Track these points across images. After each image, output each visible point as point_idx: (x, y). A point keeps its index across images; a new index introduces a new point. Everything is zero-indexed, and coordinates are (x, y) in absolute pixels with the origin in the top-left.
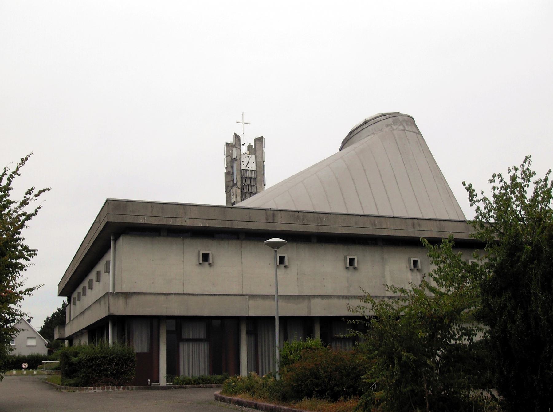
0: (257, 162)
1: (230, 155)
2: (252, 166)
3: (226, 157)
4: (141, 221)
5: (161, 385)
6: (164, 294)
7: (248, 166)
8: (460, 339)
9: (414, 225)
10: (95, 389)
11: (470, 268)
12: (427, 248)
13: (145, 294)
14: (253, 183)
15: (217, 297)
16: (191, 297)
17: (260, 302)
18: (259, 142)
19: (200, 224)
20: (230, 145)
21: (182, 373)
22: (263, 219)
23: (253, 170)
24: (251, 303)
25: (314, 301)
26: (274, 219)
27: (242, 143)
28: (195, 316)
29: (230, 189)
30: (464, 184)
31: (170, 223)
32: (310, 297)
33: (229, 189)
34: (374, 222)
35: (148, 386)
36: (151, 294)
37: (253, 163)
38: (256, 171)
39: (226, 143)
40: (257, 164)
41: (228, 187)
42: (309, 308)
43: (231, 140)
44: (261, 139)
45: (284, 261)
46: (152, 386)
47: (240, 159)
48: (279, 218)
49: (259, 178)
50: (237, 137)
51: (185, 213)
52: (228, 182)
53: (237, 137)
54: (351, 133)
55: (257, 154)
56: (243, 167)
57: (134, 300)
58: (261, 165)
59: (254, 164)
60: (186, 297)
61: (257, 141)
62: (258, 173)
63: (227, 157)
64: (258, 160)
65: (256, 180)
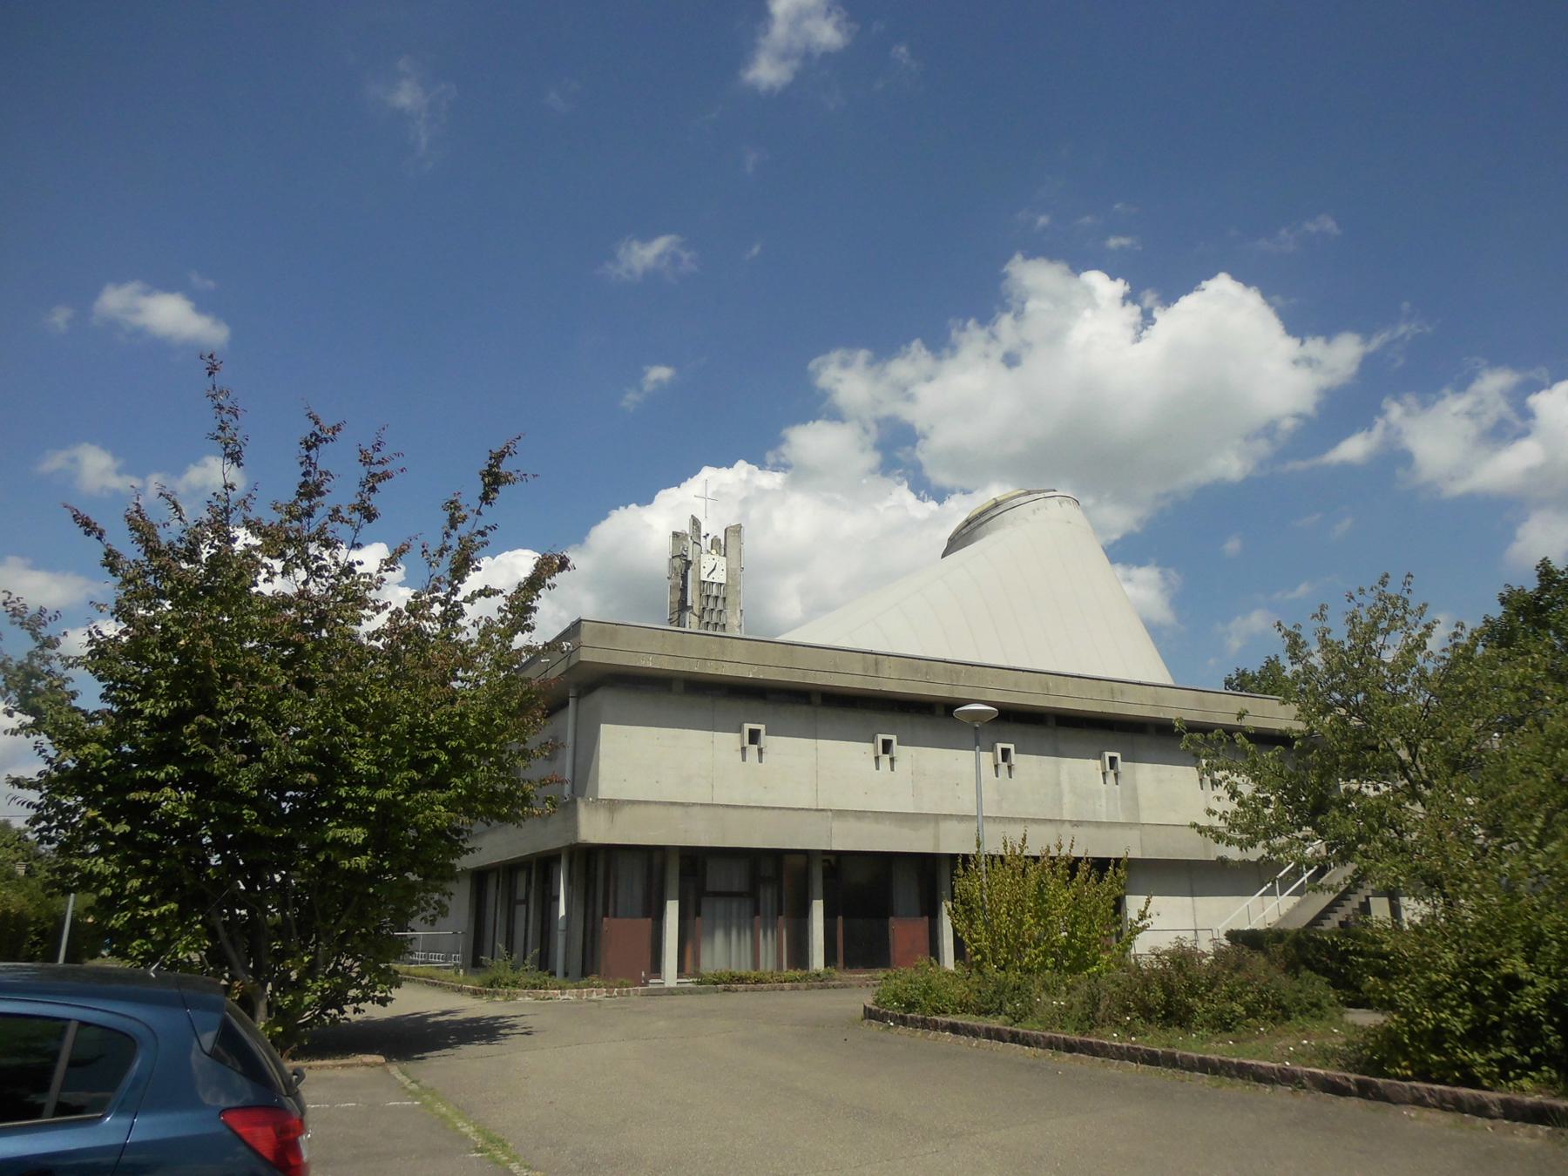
2: (720, 577)
4: (642, 663)
5: (666, 985)
6: (682, 804)
7: (711, 576)
9: (1112, 691)
10: (564, 994)
11: (546, 791)
13: (646, 803)
14: (720, 606)
15: (776, 812)
16: (731, 811)
17: (851, 824)
19: (749, 673)
22: (858, 669)
23: (721, 584)
24: (838, 826)
25: (946, 826)
26: (877, 671)
27: (703, 534)
31: (696, 669)
32: (937, 818)
34: (1047, 684)
36: (656, 803)
38: (727, 585)
42: (937, 838)
43: (686, 528)
45: (595, 755)
46: (650, 986)
47: (699, 561)
48: (888, 670)
50: (695, 522)
51: (723, 653)
53: (695, 522)
54: (969, 523)
56: (704, 578)
57: (626, 815)
60: (721, 811)
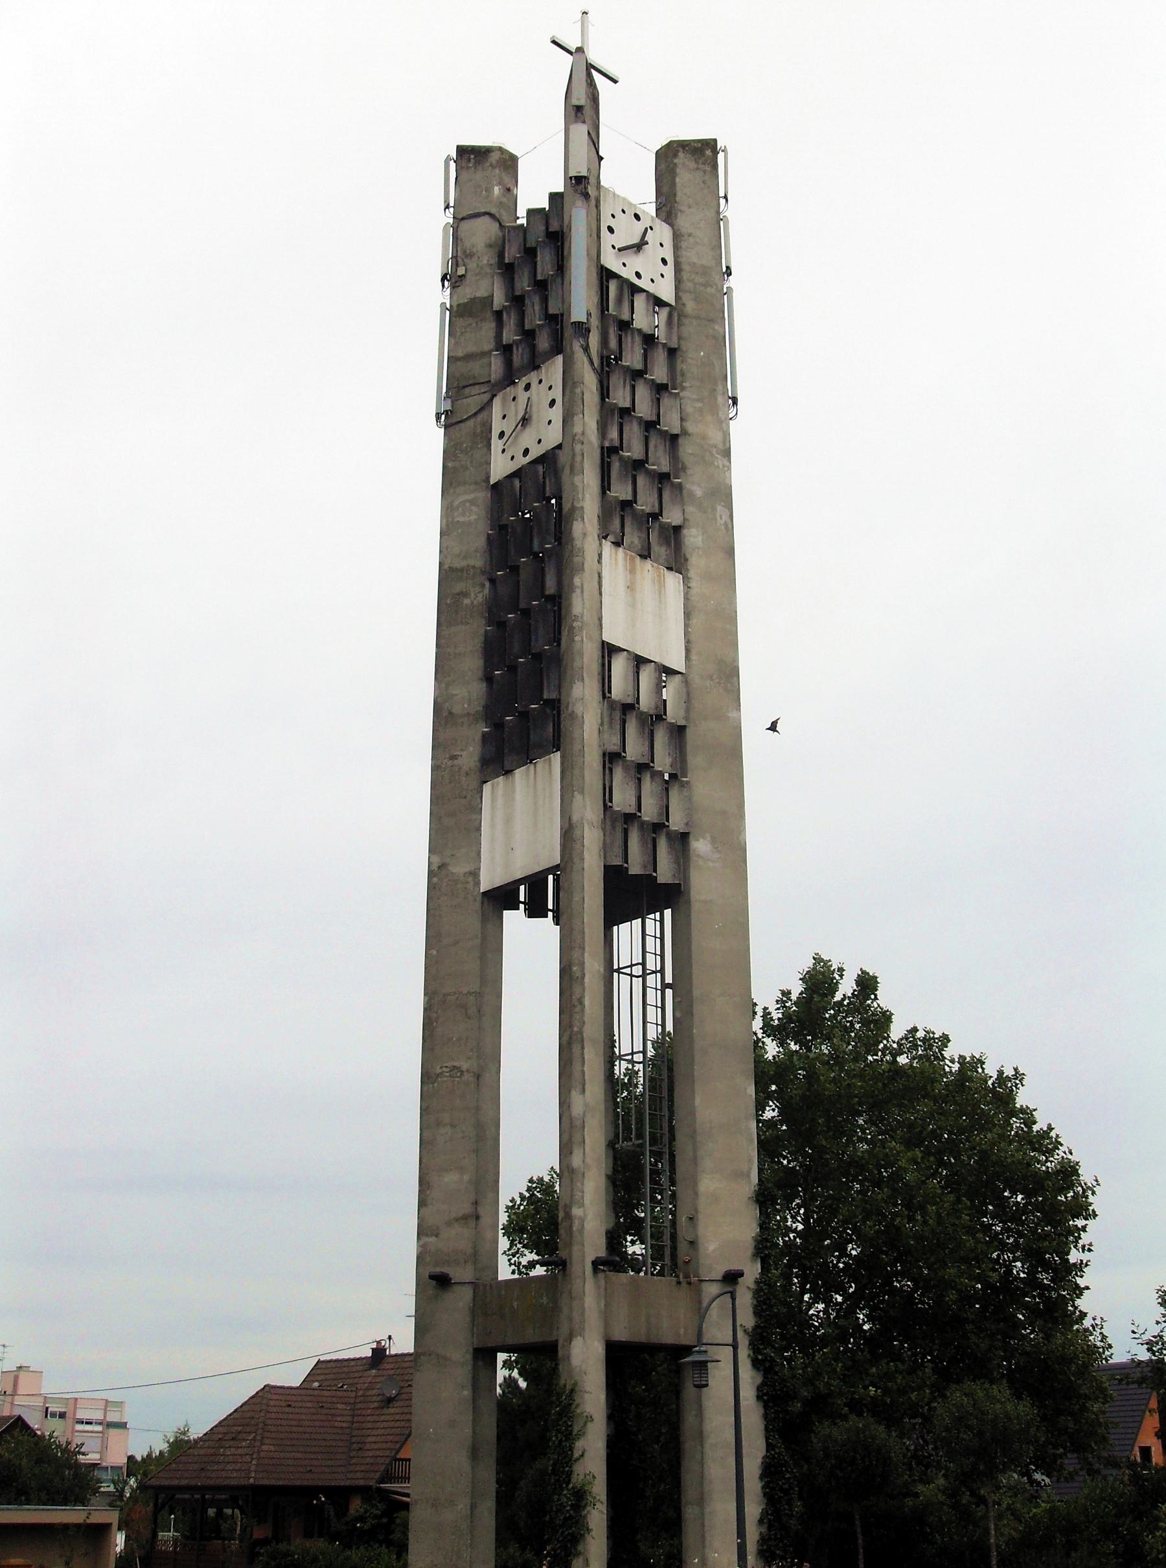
0: (686, 267)
1: (493, 211)
3: (458, 220)
8: (848, 1391)
12: (618, 1259)
18: (692, 165)
20: (494, 157)
21: (124, 1537)
28: (607, 1383)
29: (486, 397)
30: (1002, 1067)
33: (472, 402)
35: (648, 1158)
37: (664, 261)
39: (462, 151)
40: (685, 276)
41: (467, 391)
44: (708, 153)
49: (694, 358)
52: (469, 357)
55: (682, 222)
58: (707, 285)
59: (669, 271)
61: (681, 155)
62: (690, 328)
63: (465, 226)
64: (689, 256)
65: (680, 365)
